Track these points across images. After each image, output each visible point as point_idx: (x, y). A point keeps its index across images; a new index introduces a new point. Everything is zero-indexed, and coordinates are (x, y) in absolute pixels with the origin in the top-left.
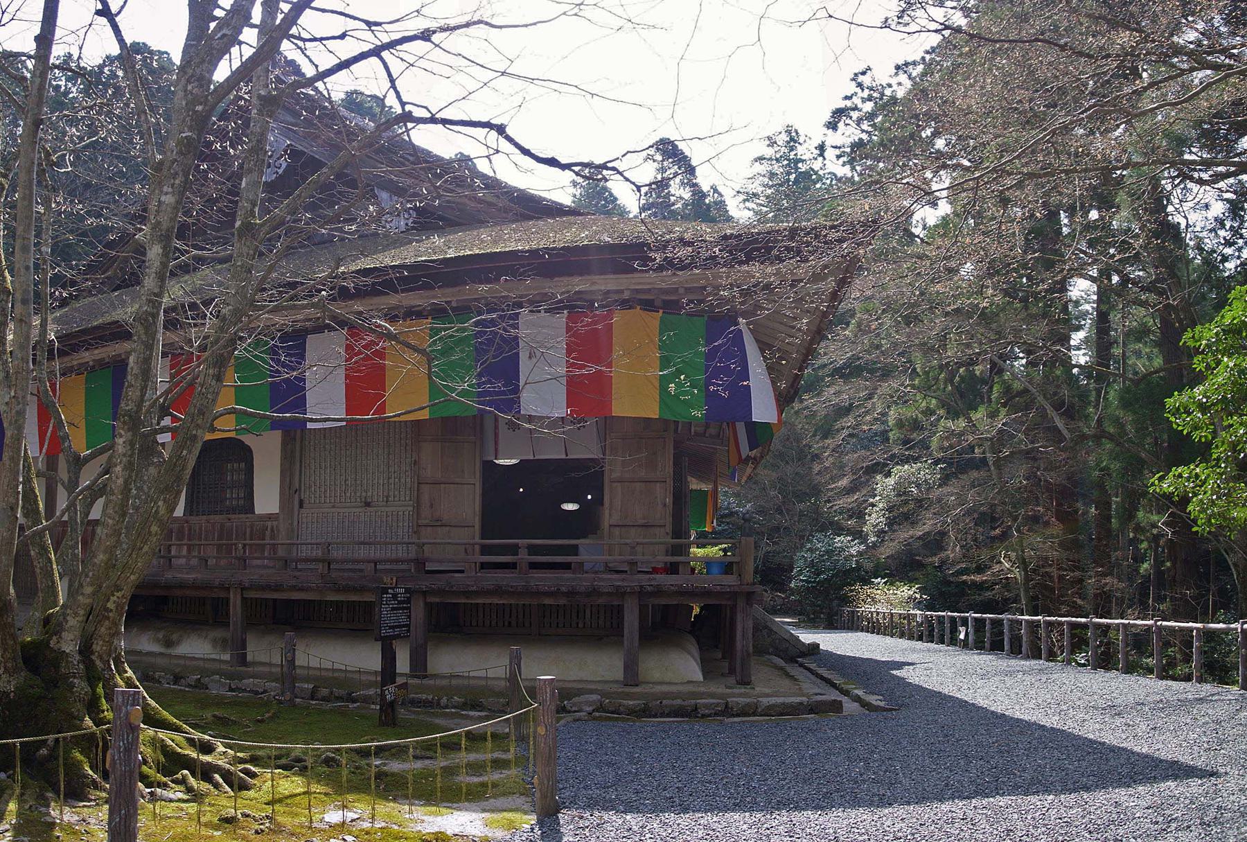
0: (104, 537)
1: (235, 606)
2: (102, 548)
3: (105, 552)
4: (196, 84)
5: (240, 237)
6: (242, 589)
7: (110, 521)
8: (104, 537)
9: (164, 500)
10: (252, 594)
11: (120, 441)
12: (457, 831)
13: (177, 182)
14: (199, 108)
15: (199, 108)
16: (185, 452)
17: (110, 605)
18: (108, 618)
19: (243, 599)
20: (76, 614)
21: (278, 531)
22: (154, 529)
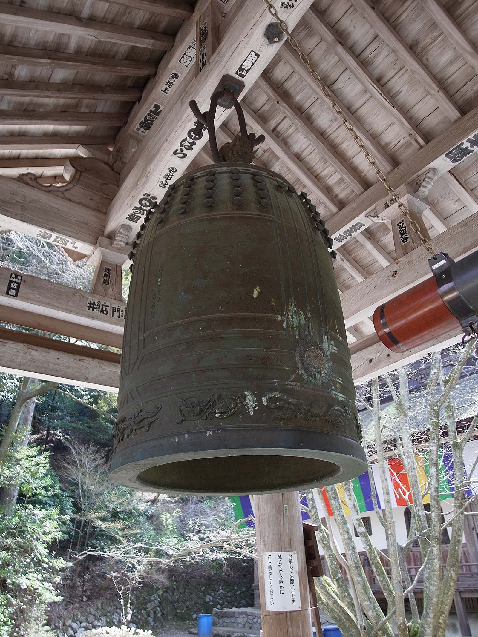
0: (434, 590)
1: (458, 605)
2: (435, 596)
3: (436, 597)
4: (431, 396)
5: (454, 449)
6: (460, 592)
7: (436, 583)
8: (434, 590)
9: (454, 571)
10: (467, 595)
11: (435, 549)
12: (426, 215)
13: (435, 441)
14: (435, 408)
15: (435, 408)
16: (457, 548)
17: (441, 621)
18: (441, 627)
19: (462, 598)
20: (430, 627)
21: (469, 554)
22: (452, 584)
